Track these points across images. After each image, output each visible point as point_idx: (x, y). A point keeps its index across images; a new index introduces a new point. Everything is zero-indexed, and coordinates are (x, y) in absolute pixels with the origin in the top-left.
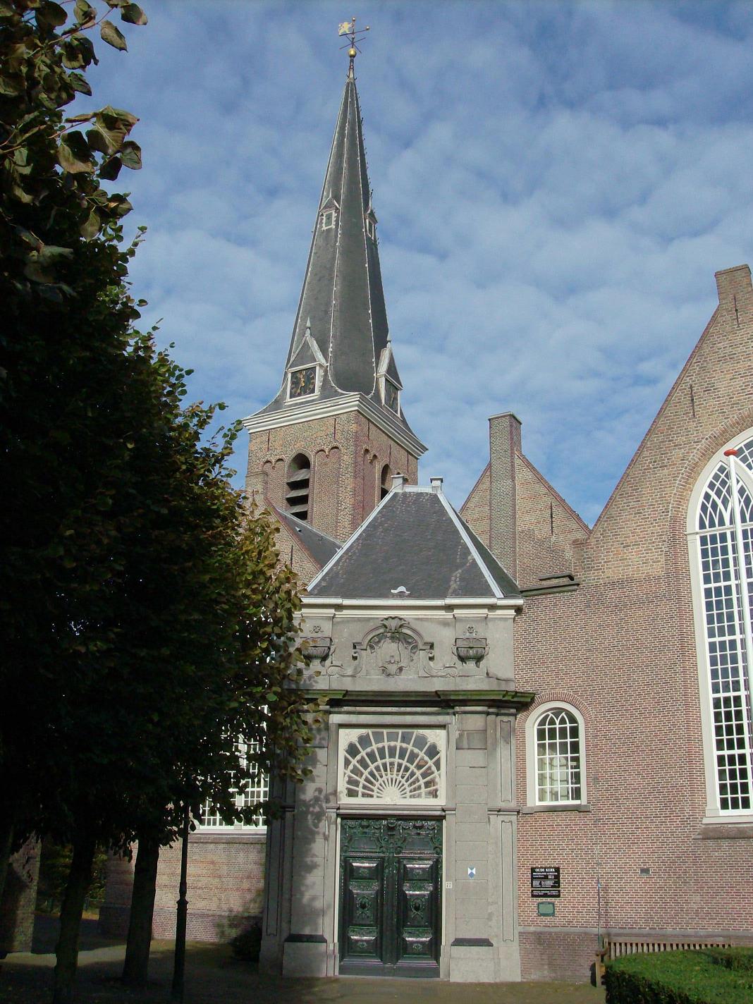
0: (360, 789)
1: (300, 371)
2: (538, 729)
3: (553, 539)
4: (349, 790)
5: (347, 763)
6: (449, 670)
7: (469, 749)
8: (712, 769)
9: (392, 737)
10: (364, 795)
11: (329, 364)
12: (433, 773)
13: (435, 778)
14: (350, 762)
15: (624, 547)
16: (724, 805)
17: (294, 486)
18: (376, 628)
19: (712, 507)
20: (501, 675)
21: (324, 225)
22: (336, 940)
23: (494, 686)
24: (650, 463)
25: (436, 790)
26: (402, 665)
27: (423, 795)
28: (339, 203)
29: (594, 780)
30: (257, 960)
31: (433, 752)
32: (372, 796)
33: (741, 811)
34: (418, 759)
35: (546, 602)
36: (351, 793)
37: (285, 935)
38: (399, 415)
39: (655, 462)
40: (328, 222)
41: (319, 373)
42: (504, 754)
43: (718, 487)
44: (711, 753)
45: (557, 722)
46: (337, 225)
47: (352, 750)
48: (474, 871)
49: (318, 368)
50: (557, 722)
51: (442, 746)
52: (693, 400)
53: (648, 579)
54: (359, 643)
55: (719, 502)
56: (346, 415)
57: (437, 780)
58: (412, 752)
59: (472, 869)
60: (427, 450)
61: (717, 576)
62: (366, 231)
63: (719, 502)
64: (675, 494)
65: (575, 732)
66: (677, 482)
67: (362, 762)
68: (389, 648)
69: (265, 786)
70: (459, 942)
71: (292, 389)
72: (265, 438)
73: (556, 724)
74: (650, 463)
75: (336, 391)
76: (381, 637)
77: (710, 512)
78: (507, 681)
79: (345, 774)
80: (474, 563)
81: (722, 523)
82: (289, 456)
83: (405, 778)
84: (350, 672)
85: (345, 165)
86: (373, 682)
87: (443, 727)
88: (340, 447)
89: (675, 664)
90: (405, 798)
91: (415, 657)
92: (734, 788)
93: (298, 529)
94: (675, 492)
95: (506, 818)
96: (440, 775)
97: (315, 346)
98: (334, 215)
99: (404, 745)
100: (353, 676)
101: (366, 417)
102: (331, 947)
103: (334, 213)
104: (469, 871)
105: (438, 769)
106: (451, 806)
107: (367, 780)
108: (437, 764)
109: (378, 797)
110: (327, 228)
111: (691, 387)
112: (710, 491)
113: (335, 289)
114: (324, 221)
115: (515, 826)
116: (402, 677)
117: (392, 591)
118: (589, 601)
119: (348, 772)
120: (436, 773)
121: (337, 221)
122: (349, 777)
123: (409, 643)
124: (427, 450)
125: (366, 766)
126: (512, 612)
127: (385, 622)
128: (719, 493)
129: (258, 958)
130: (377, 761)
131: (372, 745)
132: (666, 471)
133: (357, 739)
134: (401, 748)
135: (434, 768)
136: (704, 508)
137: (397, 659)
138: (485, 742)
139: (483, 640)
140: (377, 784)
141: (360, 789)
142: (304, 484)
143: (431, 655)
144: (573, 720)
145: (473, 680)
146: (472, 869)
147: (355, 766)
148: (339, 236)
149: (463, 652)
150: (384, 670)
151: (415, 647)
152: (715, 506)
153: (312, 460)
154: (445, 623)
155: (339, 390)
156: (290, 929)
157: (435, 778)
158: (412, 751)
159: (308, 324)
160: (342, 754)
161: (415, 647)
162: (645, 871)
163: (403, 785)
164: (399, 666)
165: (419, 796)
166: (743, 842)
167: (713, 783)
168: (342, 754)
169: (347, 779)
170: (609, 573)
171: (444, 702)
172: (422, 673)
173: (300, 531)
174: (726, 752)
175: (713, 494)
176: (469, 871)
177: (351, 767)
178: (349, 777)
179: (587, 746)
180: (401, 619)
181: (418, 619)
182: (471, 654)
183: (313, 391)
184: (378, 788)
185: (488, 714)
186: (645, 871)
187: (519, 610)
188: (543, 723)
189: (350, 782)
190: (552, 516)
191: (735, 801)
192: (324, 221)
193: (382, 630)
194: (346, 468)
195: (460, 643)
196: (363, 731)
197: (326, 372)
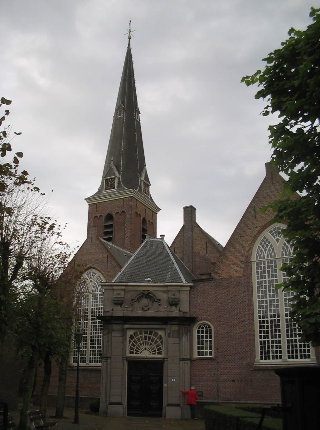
0: (134, 351)
1: (109, 179)
2: (198, 330)
3: (207, 255)
4: (130, 351)
5: (130, 342)
6: (166, 309)
7: (173, 337)
8: (258, 345)
9: (146, 333)
10: (136, 353)
11: (120, 176)
12: (160, 345)
13: (161, 347)
14: (131, 341)
15: (229, 265)
16: (289, 358)
17: (107, 227)
18: (140, 294)
19: (259, 252)
20: (184, 311)
21: (118, 115)
22: (126, 404)
23: (182, 315)
24: (239, 235)
25: (161, 352)
26: (149, 307)
27: (157, 353)
28: (124, 106)
29: (217, 349)
30: (98, 411)
31: (161, 337)
32: (139, 354)
33: (279, 360)
34: (151, 338)
35: (201, 285)
36: (131, 353)
37: (108, 402)
38: (149, 197)
39: (241, 234)
40: (120, 115)
41: (117, 180)
42: (186, 339)
43: (267, 241)
44: (258, 340)
45: (204, 328)
46: (124, 116)
47: (131, 337)
48: (174, 380)
49: (116, 178)
50: (204, 328)
51: (163, 336)
52: (255, 211)
53: (237, 277)
54: (134, 299)
55: (263, 250)
56: (127, 198)
57: (162, 348)
58: (153, 338)
59: (173, 380)
60: (161, 210)
61: (261, 277)
62: (136, 117)
63: (263, 250)
64: (248, 247)
65: (210, 332)
66: (249, 242)
67: (150, 338)
68: (145, 301)
69: (292, 303)
70: (169, 405)
71: (105, 186)
72: (95, 206)
73: (204, 328)
74: (239, 235)
75: (124, 188)
76: (142, 297)
77: (260, 254)
78: (186, 313)
79: (129, 346)
80: (176, 269)
81: (264, 257)
82: (104, 214)
83: (152, 349)
84: (131, 309)
85: (127, 89)
86: (139, 313)
87: (164, 329)
88: (125, 211)
89: (246, 308)
90: (150, 354)
91: (154, 304)
92: (277, 352)
93: (109, 247)
94: (247, 246)
95: (186, 362)
96: (162, 346)
97: (114, 168)
98: (122, 111)
99: (150, 336)
100: (132, 311)
101: (135, 199)
102: (125, 406)
103: (122, 110)
104: (173, 380)
105: (162, 344)
106: (166, 357)
107: (138, 345)
108: (162, 342)
109: (141, 354)
110: (120, 116)
111: (255, 207)
112: (260, 246)
113: (123, 144)
114: (118, 114)
115: (189, 365)
116: (149, 311)
117: (146, 280)
118: (216, 285)
119: (130, 345)
120: (161, 346)
121: (123, 114)
122: (131, 347)
123: (151, 299)
124: (161, 210)
125: (146, 339)
126: (189, 288)
127: (143, 292)
128: (263, 246)
129: (99, 407)
130: (140, 341)
131: (138, 336)
132: (244, 238)
133: (133, 333)
134: (149, 336)
135: (160, 344)
136: (258, 252)
137: (147, 305)
138: (179, 335)
139: (178, 299)
140: (140, 349)
141: (134, 351)
142: (111, 226)
143: (159, 304)
144: (210, 327)
145: (175, 312)
146: (173, 380)
147: (132, 343)
148: (124, 120)
149: (171, 302)
150: (143, 309)
151: (154, 301)
152: (261, 251)
153: (114, 216)
154: (164, 292)
155: (125, 188)
156: (110, 400)
157: (161, 347)
158: (153, 338)
159: (112, 159)
160: (128, 339)
161: (154, 301)
162: (234, 381)
163: (150, 350)
164: (148, 307)
165: (155, 354)
166: (267, 372)
167: (258, 350)
168: (128, 339)
169: (130, 347)
170: (223, 275)
171: (165, 321)
172: (156, 310)
173: (110, 248)
174: (290, 338)
175: (261, 247)
176: (173, 380)
177: (131, 343)
178: (131, 347)
179: (215, 336)
180: (149, 291)
181: (154, 290)
182: (174, 303)
183: (114, 188)
184: (142, 350)
185: (180, 325)
186: (234, 381)
187: (191, 287)
188: (199, 328)
189: (131, 348)
190: (207, 247)
191: (293, 356)
192: (118, 114)
193: (142, 295)
194: (128, 220)
195: (170, 299)
196: (135, 331)
197: (119, 179)
